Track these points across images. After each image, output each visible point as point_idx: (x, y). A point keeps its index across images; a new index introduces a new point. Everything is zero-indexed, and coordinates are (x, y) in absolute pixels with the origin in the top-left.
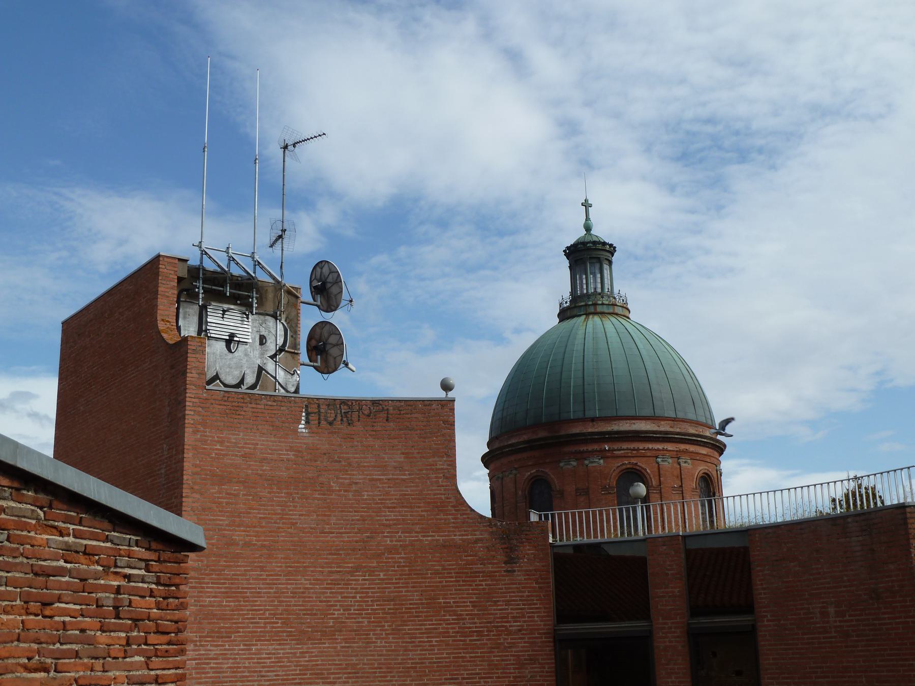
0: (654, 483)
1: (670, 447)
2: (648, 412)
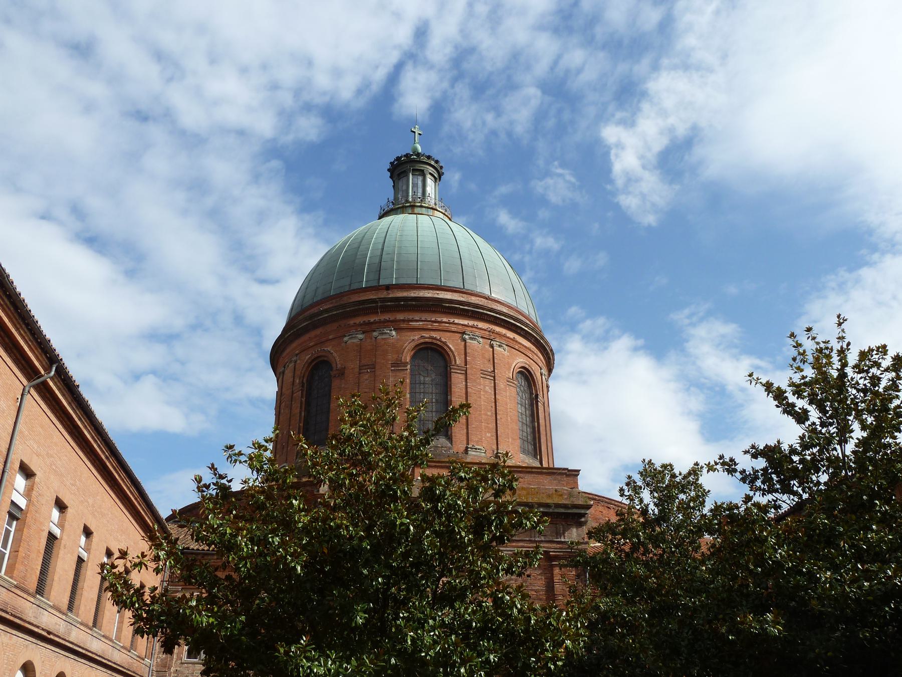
2: (458, 284)
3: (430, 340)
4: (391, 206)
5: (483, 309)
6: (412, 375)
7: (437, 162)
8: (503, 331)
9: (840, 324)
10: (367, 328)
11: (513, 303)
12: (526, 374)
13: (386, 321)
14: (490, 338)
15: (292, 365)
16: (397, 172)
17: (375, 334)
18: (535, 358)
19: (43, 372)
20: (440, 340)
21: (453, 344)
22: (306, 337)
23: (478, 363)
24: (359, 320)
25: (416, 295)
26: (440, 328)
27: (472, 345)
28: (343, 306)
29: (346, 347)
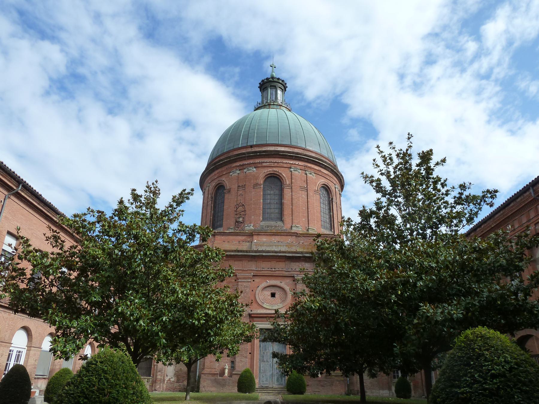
0: (288, 183)
1: (301, 163)
2: (287, 142)
4: (259, 106)
6: (264, 190)
7: (283, 81)
8: (313, 166)
9: (409, 138)
10: (241, 168)
11: (319, 152)
12: (326, 188)
13: (250, 164)
16: (262, 88)
17: (245, 170)
18: (331, 179)
19: (15, 188)
20: (278, 172)
21: (284, 173)
24: (238, 164)
27: (294, 173)
28: (230, 157)
29: (231, 178)
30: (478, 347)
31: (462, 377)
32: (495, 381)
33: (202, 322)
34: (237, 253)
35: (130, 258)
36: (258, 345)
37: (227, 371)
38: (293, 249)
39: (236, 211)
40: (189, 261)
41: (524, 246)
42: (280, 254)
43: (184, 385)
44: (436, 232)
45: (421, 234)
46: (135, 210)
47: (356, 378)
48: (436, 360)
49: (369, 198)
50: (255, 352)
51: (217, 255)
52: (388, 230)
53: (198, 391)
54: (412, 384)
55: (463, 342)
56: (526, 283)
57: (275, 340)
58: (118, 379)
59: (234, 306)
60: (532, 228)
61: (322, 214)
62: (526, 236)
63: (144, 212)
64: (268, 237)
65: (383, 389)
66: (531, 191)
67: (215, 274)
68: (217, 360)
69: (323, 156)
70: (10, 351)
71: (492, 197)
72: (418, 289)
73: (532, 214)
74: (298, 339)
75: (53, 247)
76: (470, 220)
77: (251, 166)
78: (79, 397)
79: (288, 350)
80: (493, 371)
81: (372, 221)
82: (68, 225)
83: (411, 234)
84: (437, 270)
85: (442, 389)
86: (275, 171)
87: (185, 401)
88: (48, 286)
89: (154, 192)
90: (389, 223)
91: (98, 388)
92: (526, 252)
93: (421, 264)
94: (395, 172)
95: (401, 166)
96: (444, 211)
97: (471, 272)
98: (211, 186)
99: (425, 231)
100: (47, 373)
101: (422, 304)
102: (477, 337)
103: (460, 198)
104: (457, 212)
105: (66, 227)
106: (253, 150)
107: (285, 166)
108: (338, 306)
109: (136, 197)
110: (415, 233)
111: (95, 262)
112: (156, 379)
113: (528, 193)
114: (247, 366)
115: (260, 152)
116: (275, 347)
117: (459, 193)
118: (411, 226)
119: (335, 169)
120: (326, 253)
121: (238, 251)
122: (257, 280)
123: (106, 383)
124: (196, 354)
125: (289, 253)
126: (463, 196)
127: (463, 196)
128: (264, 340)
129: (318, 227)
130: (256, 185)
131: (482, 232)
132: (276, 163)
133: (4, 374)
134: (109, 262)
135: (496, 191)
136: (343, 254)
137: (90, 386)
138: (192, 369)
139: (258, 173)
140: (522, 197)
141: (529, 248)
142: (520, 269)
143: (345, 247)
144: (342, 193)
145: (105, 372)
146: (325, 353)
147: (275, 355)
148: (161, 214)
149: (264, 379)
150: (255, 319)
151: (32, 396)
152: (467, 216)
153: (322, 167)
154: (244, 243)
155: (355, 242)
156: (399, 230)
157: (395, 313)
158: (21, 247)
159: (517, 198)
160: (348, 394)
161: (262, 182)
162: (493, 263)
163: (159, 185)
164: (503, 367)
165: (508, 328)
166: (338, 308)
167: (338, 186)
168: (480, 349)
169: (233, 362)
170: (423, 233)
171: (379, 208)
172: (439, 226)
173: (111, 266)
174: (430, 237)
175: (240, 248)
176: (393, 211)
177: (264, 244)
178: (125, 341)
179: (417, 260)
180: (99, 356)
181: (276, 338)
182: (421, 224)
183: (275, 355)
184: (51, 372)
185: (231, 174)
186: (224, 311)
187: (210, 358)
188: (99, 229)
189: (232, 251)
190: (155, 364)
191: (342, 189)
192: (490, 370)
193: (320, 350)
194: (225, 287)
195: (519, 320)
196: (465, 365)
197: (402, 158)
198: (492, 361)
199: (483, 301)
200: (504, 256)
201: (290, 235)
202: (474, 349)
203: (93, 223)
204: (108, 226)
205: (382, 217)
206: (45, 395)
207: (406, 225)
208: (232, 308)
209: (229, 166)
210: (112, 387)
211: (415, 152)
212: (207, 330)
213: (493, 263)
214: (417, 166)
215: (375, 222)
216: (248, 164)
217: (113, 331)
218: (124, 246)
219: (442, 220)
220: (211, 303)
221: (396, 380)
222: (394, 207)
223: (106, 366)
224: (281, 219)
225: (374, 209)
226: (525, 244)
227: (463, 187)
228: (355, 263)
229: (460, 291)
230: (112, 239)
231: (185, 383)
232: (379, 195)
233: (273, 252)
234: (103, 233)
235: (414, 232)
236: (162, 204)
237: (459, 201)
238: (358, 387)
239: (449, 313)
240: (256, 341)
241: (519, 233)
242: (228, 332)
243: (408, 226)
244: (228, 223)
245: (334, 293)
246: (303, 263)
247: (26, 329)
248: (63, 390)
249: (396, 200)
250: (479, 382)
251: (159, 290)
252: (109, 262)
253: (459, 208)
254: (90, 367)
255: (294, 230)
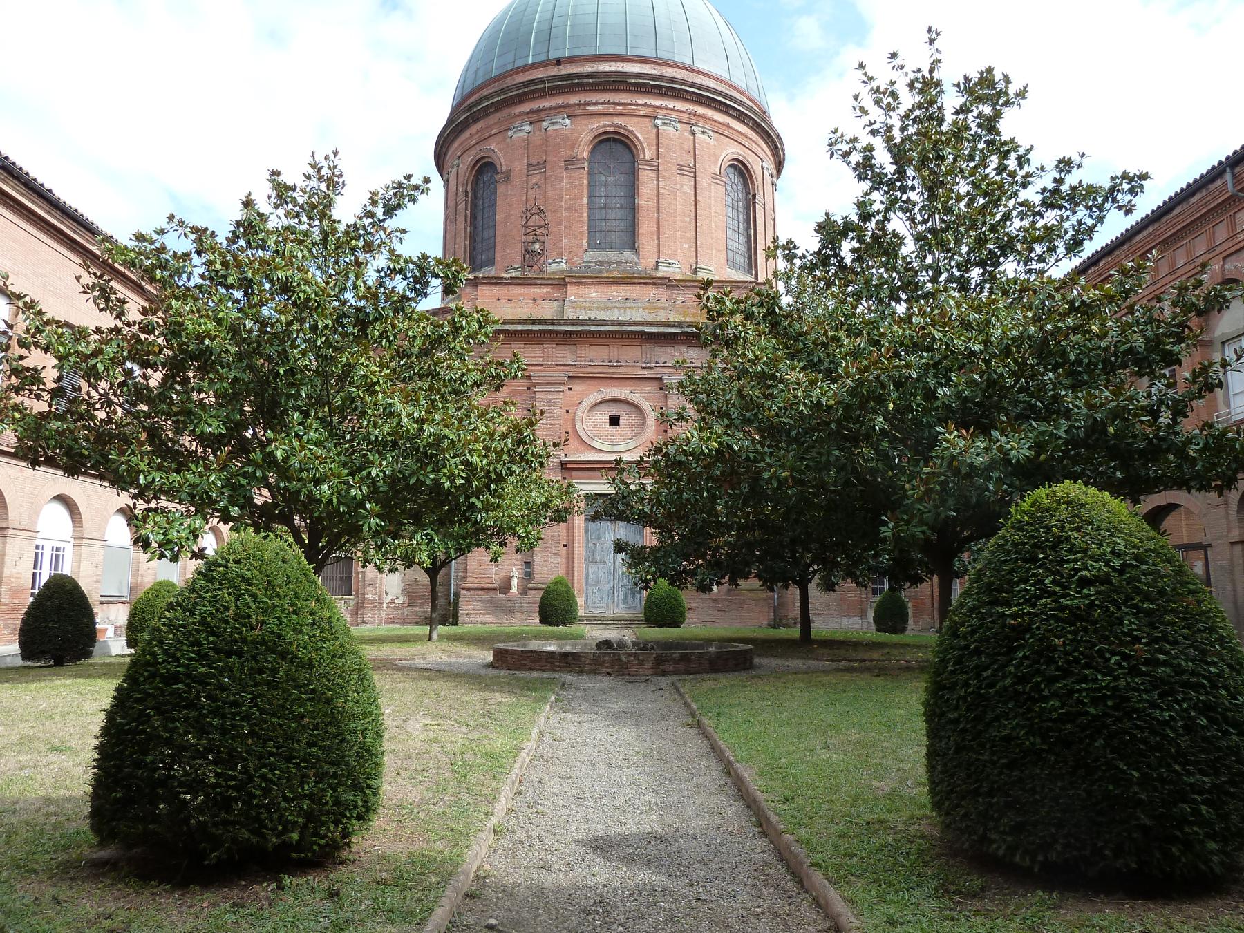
0: (648, 156)
1: (681, 105)
2: (647, 52)
3: (612, 129)
5: (681, 84)
6: (590, 174)
8: (710, 113)
9: (932, 41)
10: (535, 117)
11: (724, 75)
12: (741, 169)
14: (689, 122)
15: (454, 170)
17: (544, 124)
20: (625, 128)
21: (640, 131)
22: (466, 134)
23: (674, 155)
24: (526, 107)
25: (594, 70)
26: (625, 112)
27: (664, 132)
28: (505, 91)
29: (510, 143)
30: (1059, 524)
31: (1018, 583)
32: (1085, 591)
33: (459, 482)
34: (530, 327)
35: (282, 338)
36: (583, 528)
37: (515, 583)
38: (661, 316)
39: (524, 226)
40: (418, 342)
41: (1188, 308)
42: (629, 329)
43: (424, 612)
44: (992, 277)
45: (958, 280)
46: (285, 222)
47: (794, 592)
48: (966, 557)
49: (842, 194)
50: (576, 543)
51: (481, 326)
52: (882, 270)
53: (456, 624)
54: (910, 605)
55: (1027, 513)
56: (1181, 389)
57: (619, 517)
58: (278, 596)
59: (525, 443)
60: (1215, 266)
61: (730, 232)
62: (1199, 284)
63: (305, 227)
64: (601, 287)
65: (849, 616)
66: (1228, 176)
67: (482, 372)
68: (494, 560)
69: (735, 88)
70: (37, 547)
71: (1132, 191)
72: (938, 403)
73: (1221, 233)
74: (669, 515)
75: (101, 310)
76: (1074, 246)
77: (558, 114)
78: (198, 631)
79: (649, 538)
80: (1084, 573)
81: (847, 248)
82: (125, 263)
83: (934, 280)
84: (984, 360)
85: (972, 610)
86: (616, 126)
87: (429, 644)
88: (98, 406)
89: (328, 179)
90: (886, 253)
91: (236, 614)
92: (1194, 322)
93: (947, 344)
94: (903, 129)
95: (918, 112)
96: (1017, 223)
97: (1062, 365)
98: (463, 164)
99: (967, 271)
100: (126, 592)
101: (940, 430)
102: (1059, 503)
103: (1056, 191)
104: (1045, 227)
105: (121, 269)
106: (563, 72)
107: (642, 113)
108: (760, 443)
109: (282, 192)
110: (944, 276)
111: (202, 347)
112: (364, 599)
113: (1219, 182)
114: (560, 572)
115: (580, 76)
116: (622, 531)
117: (1055, 180)
118: (936, 261)
119: (763, 120)
120: (733, 322)
121: (533, 322)
122: (578, 387)
123: (252, 604)
124: (447, 548)
125: (651, 324)
126: (1065, 188)
127: (1065, 188)
128: (596, 518)
129: (719, 265)
130: (572, 162)
131: (1100, 275)
132: (619, 104)
133: (32, 594)
134: (233, 350)
135: (1144, 177)
136: (774, 325)
137: (217, 610)
138: (440, 579)
139: (579, 133)
140: (1204, 192)
141: (1200, 313)
142: (1172, 360)
143: (781, 309)
144: (780, 183)
145: (246, 580)
146: (727, 544)
147: (619, 547)
148: (347, 233)
149: (597, 599)
150: (574, 473)
151: (99, 638)
152: (1068, 237)
153: (731, 116)
154: (546, 304)
155: (805, 298)
156: (907, 270)
157: (884, 457)
158: (21, 317)
159: (1193, 194)
160: (774, 626)
161: (586, 155)
162: (1115, 346)
163: (342, 164)
164: (1107, 563)
165: (1131, 489)
166: (758, 446)
167: (769, 164)
168: (1062, 528)
169: (527, 564)
170: (962, 276)
171: (866, 217)
172: (1002, 259)
173: (239, 357)
174: (977, 285)
175: (537, 315)
176: (898, 224)
177: (591, 304)
178: (288, 522)
179: (938, 335)
180: (230, 549)
181: (622, 512)
182: (960, 255)
183: (619, 547)
184: (133, 589)
185: (510, 133)
186: (505, 457)
187: (477, 557)
188: (201, 270)
189: (519, 322)
190: (360, 569)
191: (779, 172)
192: (1077, 570)
193: (716, 537)
194: (505, 403)
195: (1156, 472)
196: (1026, 561)
197: (922, 92)
198: (1086, 551)
199: (1078, 428)
200: (1142, 331)
201: (654, 284)
202: (1048, 528)
203: (186, 256)
204: (222, 264)
205: (872, 237)
206: (127, 636)
207: (925, 257)
208: (521, 448)
209: (505, 112)
210: (265, 611)
211: (949, 75)
212: (467, 498)
213: (1115, 346)
214: (957, 113)
215: (853, 251)
216: (551, 108)
217: (259, 501)
218: (265, 311)
219: (1007, 248)
220: (476, 440)
221: (878, 598)
222: (900, 214)
223: (248, 570)
224: (633, 245)
225: (854, 218)
226: (1193, 304)
227: (1065, 165)
228: (801, 345)
229: (1033, 407)
230: (235, 293)
231: (428, 607)
232: (866, 185)
233: (613, 323)
234: (211, 279)
235: (941, 273)
236: (346, 210)
237: (1053, 199)
238: (795, 611)
239: (1000, 449)
240: (578, 521)
241: (1184, 278)
242: (514, 500)
243: (929, 260)
244: (508, 256)
245: (749, 414)
246: (683, 349)
247: (63, 499)
248: (160, 618)
249: (904, 197)
250: (1051, 593)
251: (355, 409)
252: (233, 350)
253: (1051, 217)
254: (211, 571)
255: (663, 271)
